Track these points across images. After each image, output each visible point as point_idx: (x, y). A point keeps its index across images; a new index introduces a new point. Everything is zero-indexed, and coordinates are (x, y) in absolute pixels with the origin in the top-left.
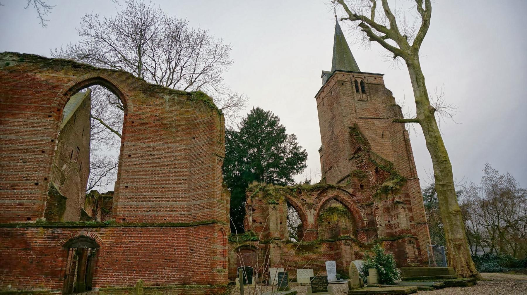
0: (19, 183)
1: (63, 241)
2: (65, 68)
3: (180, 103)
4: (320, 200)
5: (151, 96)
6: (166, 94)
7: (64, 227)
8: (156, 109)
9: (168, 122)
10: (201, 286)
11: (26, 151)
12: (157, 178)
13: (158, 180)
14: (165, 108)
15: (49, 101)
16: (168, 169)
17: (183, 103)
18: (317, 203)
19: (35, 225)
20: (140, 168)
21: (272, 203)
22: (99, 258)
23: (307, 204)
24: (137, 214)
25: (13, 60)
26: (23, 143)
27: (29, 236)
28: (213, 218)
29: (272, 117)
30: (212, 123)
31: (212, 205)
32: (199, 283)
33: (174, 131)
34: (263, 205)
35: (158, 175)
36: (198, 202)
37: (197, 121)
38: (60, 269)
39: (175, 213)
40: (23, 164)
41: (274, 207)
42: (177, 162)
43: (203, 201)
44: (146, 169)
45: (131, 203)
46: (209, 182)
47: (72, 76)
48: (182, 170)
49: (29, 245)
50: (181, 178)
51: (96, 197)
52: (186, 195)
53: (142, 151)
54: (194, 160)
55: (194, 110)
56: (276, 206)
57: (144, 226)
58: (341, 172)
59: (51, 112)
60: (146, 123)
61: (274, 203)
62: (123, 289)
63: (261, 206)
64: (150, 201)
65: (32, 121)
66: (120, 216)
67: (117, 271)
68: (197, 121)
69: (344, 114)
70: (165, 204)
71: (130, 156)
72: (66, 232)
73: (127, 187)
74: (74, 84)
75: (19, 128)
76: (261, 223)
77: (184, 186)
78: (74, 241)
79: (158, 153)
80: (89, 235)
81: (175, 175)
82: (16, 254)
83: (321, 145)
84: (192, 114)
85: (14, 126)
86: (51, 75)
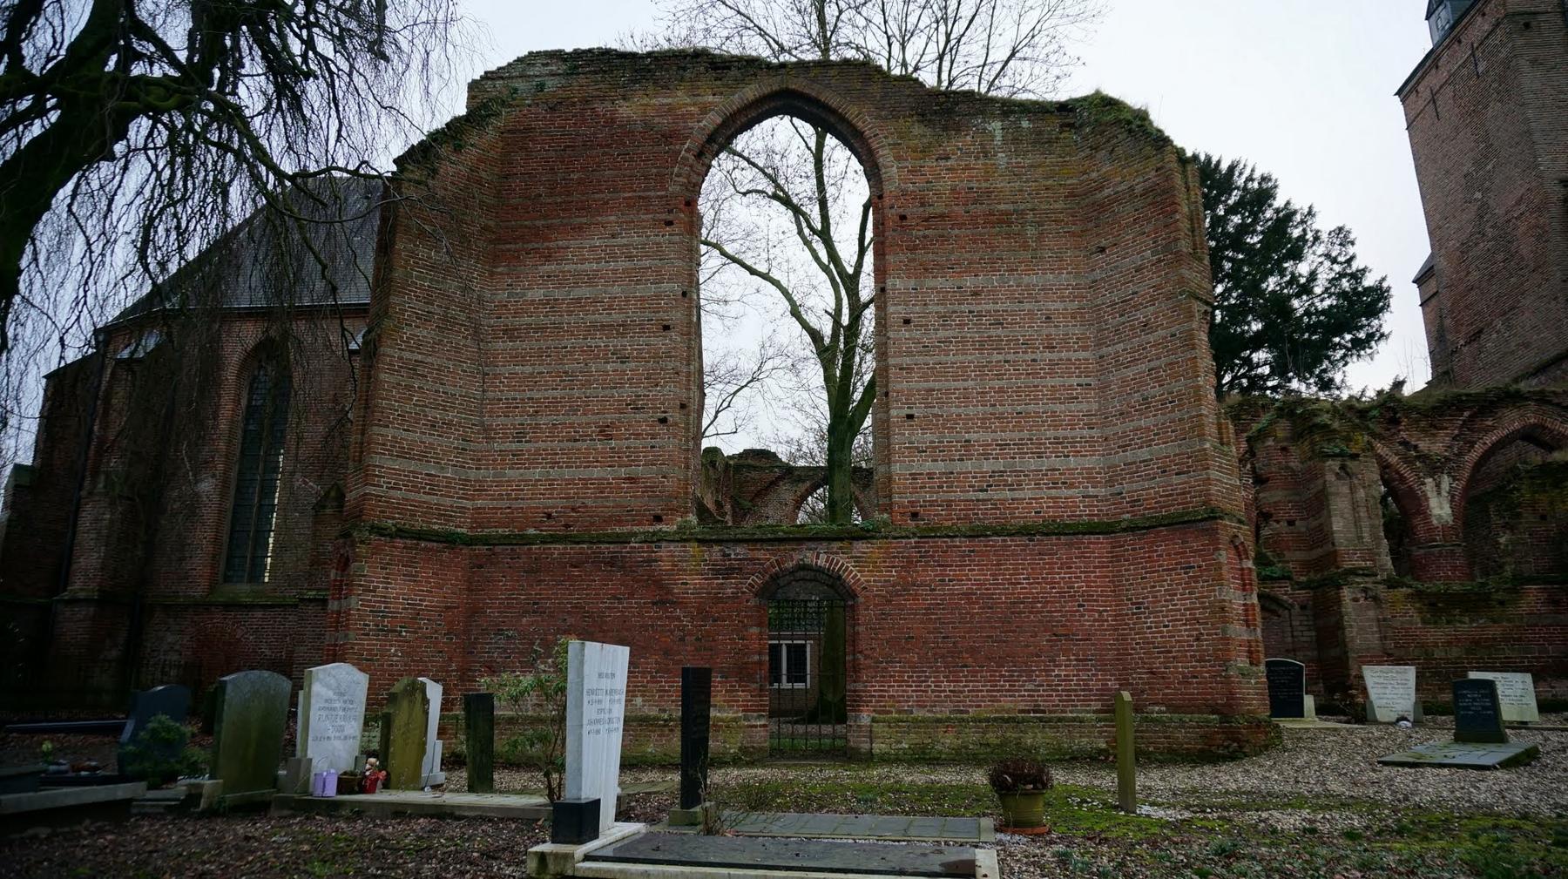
0: (619, 420)
1: (756, 580)
2: (688, 74)
3: (1040, 141)
4: (1472, 444)
5: (945, 129)
6: (993, 116)
7: (751, 541)
8: (967, 167)
9: (1011, 207)
10: (1186, 718)
11: (622, 329)
12: (997, 384)
13: (1001, 390)
14: (996, 164)
15: (661, 180)
16: (1029, 357)
17: (1049, 142)
18: (1460, 455)
19: (677, 537)
20: (943, 358)
21: (1335, 456)
22: (861, 629)
23: (1423, 457)
24: (952, 496)
25: (553, 75)
26: (611, 308)
27: (665, 565)
28: (1204, 503)
29: (1250, 179)
30: (1164, 192)
31: (1202, 460)
32: (1173, 708)
33: (1031, 231)
34: (1295, 464)
35: (999, 376)
36: (1144, 453)
37: (1106, 192)
38: (756, 658)
39: (1065, 492)
40: (618, 366)
41: (1343, 467)
42: (1053, 331)
43: (1160, 449)
44: (960, 358)
45: (929, 466)
46: (1177, 387)
47: (711, 98)
48: (1073, 356)
49: (669, 592)
50: (1074, 381)
51: (720, 466)
52: (1095, 433)
53: (941, 303)
54: (1113, 321)
55: (1091, 157)
56: (1349, 463)
57: (976, 534)
58: (1526, 345)
59: (670, 212)
60: (942, 216)
61: (1341, 455)
62: (938, 721)
63: (1287, 468)
64: (986, 456)
65: (625, 241)
66: (901, 506)
67: (913, 667)
68: (1106, 192)
69: (1536, 136)
70: (1032, 464)
71: (907, 322)
72: (760, 555)
73: (910, 417)
74: (719, 120)
75: (595, 266)
76: (1291, 523)
77: (1084, 407)
78: (781, 582)
79: (991, 307)
80: (822, 562)
81: (1052, 373)
82: (640, 615)
83: (1429, 251)
84: (1084, 173)
85: (583, 261)
86: (654, 101)
